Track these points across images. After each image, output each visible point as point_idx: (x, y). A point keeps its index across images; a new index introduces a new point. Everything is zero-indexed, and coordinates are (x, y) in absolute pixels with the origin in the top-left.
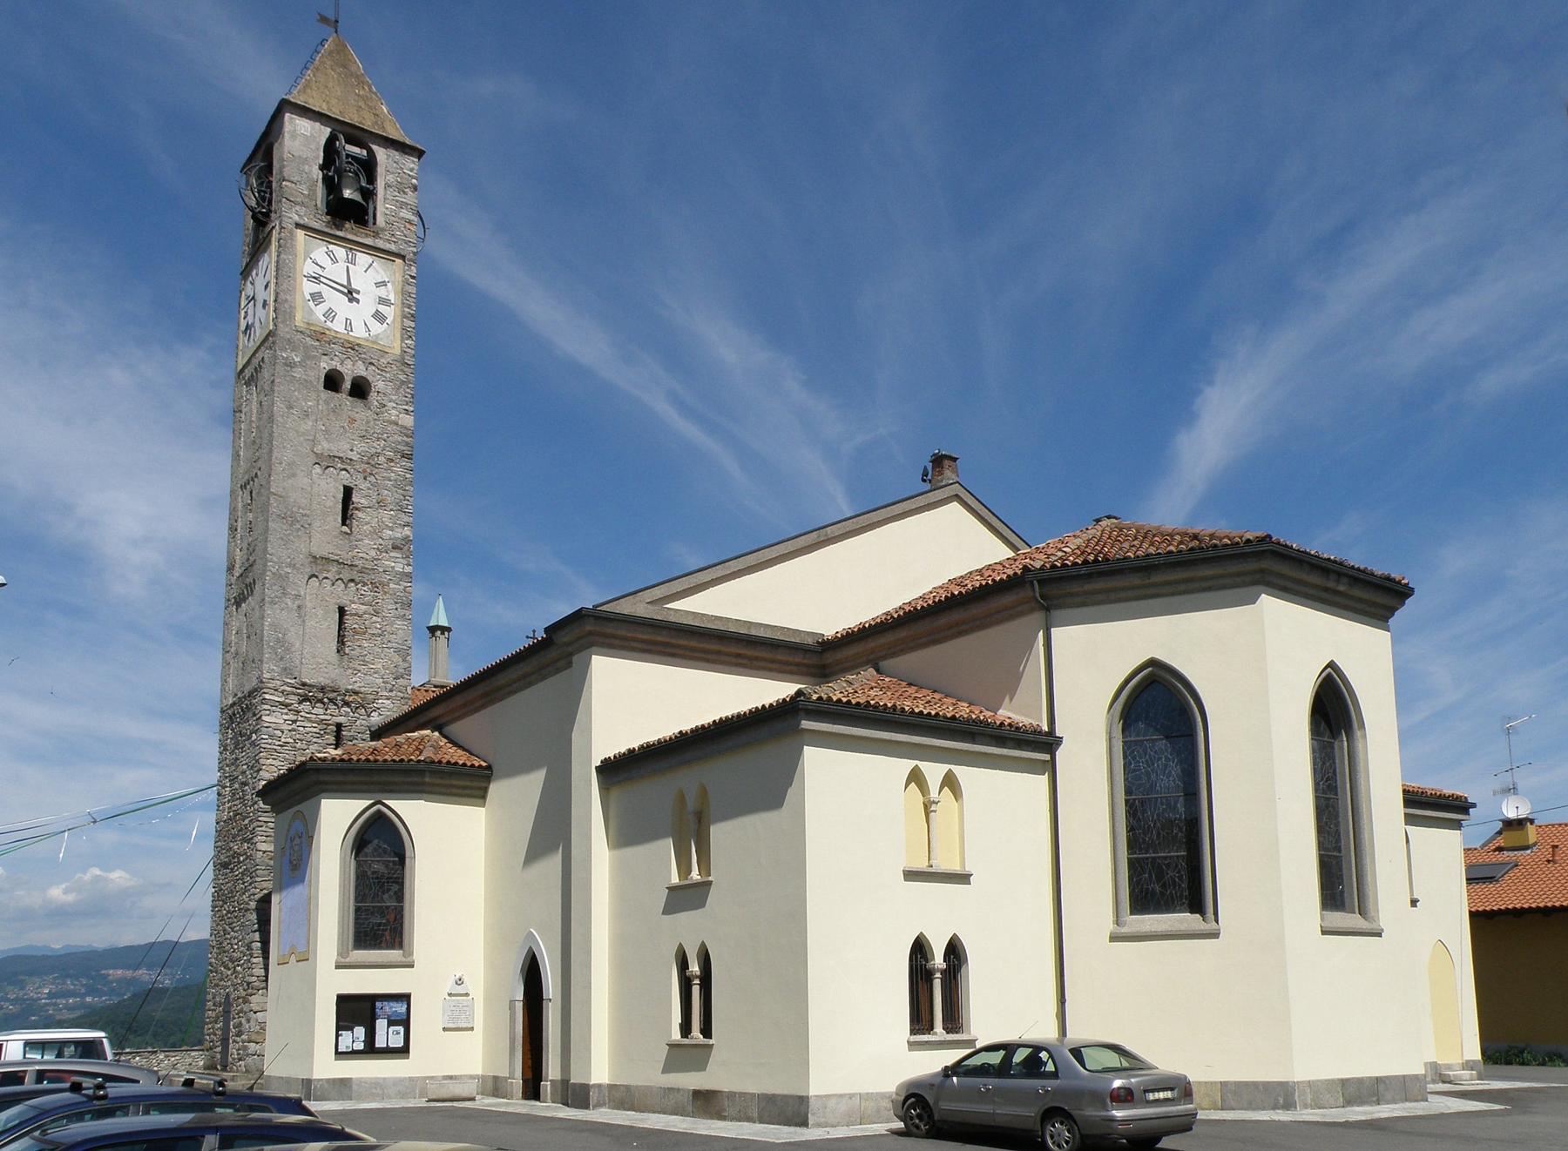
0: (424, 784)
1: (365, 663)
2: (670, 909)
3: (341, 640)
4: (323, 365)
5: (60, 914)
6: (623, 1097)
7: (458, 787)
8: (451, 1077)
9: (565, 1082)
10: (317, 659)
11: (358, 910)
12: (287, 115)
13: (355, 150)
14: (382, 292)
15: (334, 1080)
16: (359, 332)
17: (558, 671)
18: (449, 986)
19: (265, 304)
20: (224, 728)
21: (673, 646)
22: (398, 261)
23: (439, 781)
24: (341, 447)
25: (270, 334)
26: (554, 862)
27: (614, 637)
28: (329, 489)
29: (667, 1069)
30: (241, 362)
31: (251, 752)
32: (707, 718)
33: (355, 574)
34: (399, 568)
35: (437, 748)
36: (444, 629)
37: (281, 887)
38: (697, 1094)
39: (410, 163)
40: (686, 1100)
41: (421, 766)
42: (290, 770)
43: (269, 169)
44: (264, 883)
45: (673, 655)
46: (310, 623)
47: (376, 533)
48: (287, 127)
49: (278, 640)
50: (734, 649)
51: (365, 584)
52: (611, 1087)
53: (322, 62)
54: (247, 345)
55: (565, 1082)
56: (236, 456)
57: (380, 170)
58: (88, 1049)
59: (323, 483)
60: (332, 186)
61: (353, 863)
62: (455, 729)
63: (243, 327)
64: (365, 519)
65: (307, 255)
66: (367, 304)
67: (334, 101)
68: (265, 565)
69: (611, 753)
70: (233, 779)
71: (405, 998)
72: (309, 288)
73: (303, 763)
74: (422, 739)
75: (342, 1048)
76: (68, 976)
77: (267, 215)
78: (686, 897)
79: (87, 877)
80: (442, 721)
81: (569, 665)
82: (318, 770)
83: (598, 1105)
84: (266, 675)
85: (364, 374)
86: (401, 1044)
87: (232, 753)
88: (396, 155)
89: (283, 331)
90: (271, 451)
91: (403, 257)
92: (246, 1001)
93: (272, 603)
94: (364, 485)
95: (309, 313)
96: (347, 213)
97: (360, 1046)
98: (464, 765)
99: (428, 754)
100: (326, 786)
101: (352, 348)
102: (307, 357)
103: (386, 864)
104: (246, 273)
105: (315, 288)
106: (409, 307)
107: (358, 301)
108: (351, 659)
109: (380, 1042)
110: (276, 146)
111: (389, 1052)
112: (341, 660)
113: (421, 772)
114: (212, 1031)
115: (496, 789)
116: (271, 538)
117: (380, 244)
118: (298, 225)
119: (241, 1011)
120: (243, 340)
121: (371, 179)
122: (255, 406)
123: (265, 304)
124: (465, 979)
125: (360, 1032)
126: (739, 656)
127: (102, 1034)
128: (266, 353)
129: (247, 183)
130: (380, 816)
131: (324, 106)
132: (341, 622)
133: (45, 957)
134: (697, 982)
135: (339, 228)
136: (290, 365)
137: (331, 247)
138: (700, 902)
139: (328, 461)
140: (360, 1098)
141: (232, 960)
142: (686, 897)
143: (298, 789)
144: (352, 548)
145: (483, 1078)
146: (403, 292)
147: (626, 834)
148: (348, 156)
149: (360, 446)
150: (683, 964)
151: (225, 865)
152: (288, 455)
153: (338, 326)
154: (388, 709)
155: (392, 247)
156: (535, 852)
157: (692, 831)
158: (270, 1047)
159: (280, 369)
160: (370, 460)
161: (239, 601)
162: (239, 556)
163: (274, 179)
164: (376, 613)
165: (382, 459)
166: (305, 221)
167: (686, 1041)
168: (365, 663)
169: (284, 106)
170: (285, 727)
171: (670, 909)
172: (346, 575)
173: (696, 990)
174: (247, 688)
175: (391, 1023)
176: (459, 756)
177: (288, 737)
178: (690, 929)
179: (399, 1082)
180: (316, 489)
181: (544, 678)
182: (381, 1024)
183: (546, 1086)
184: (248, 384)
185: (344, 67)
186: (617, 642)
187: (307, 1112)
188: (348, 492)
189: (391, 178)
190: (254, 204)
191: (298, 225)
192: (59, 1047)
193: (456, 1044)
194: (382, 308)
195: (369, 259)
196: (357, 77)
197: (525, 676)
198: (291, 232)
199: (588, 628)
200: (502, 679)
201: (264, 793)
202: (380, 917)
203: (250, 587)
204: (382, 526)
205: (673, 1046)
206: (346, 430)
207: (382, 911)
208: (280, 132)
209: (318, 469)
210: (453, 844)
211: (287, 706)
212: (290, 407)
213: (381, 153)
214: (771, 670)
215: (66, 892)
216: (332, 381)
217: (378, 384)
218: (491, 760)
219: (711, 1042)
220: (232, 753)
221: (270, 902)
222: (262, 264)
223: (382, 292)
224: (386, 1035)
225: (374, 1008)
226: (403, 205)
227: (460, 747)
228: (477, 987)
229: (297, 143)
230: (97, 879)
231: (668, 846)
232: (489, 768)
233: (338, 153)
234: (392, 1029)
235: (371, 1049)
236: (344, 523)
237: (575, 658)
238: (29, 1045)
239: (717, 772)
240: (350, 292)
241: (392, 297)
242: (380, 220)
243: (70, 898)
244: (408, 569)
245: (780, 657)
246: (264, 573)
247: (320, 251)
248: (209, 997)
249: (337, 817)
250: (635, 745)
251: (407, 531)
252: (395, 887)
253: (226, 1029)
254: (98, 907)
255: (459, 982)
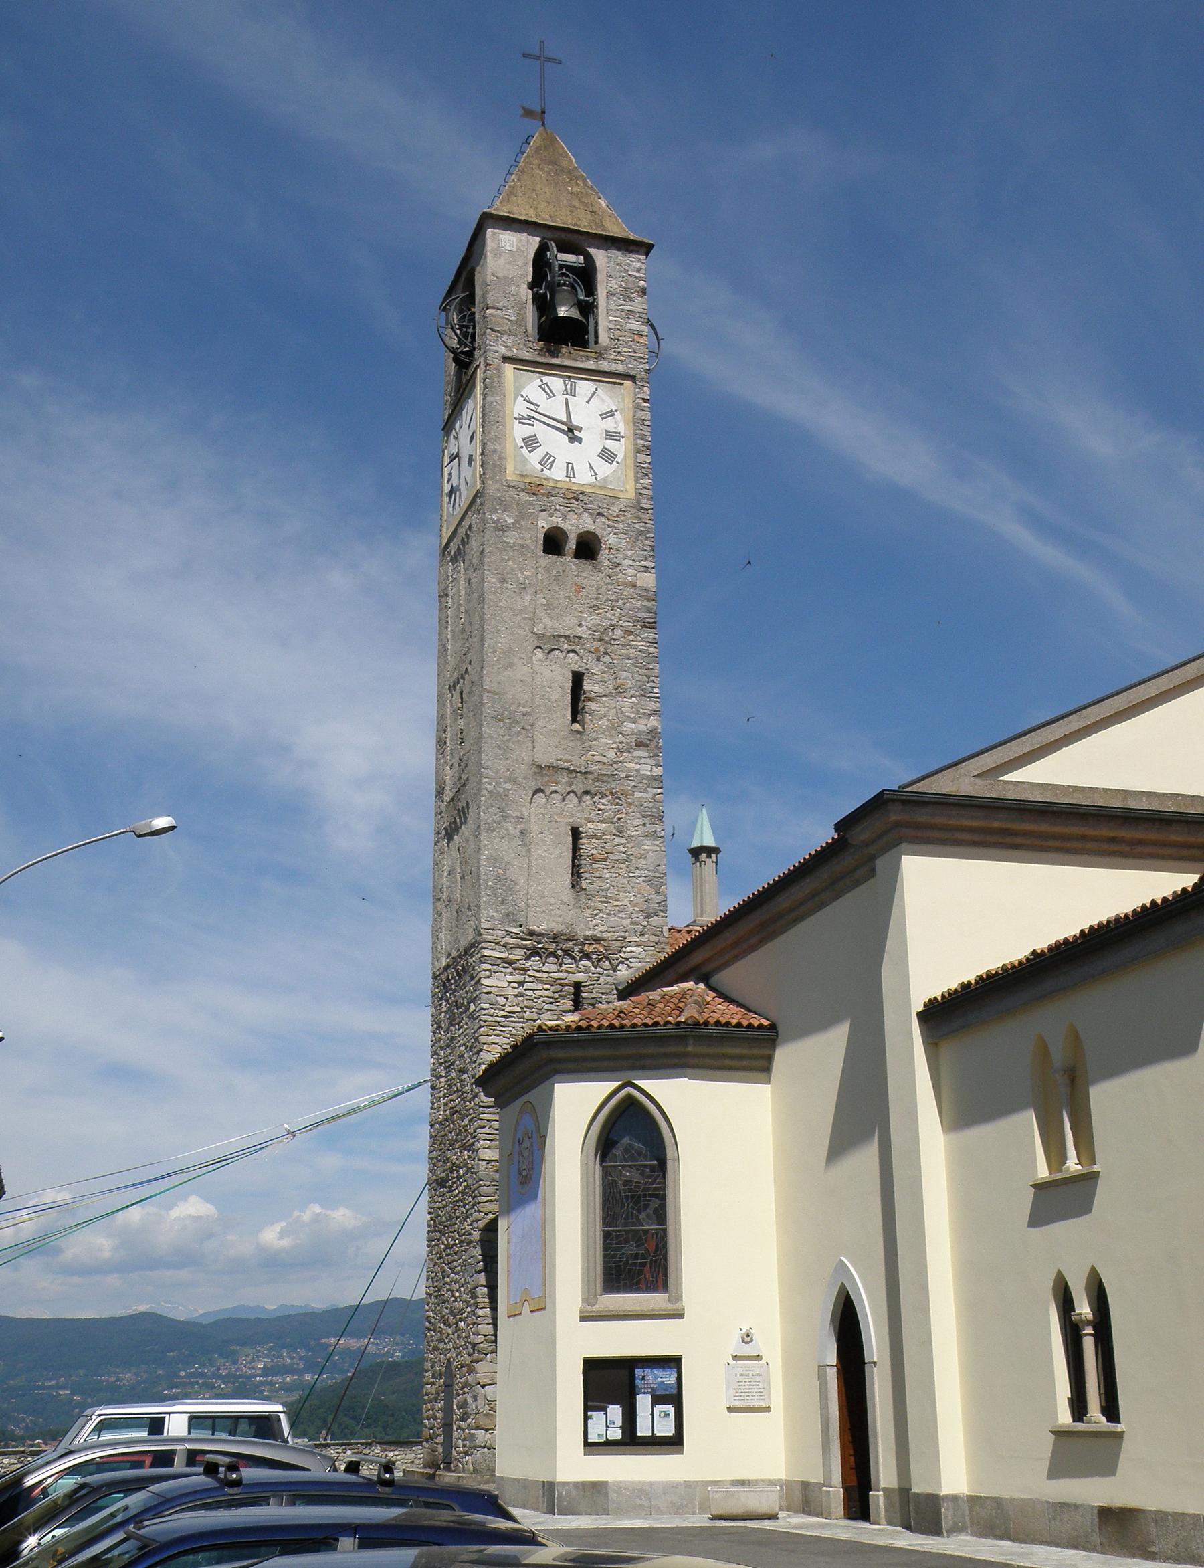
0: (686, 1055)
1: (608, 899)
2: (1039, 1217)
3: (576, 872)
4: (541, 523)
5: (273, 1264)
6: (993, 1517)
7: (732, 1057)
8: (742, 1483)
9: (904, 1492)
10: (548, 903)
11: (607, 1236)
12: (489, 231)
13: (570, 258)
14: (609, 424)
15: (584, 1484)
16: (583, 478)
17: (858, 883)
18: (734, 1345)
19: (471, 459)
20: (437, 999)
21: (1016, 833)
22: (628, 383)
23: (705, 1050)
24: (567, 623)
25: (478, 494)
26: (866, 1157)
27: (932, 827)
29: (1055, 1472)
30: (446, 534)
31: (468, 1027)
32: (1070, 928)
33: (590, 783)
34: (645, 770)
35: (702, 1005)
36: (710, 851)
37: (509, 1207)
38: (1107, 1515)
39: (636, 263)
40: (1089, 1523)
41: (682, 1030)
42: (514, 1047)
43: (471, 299)
44: (489, 1205)
45: (1016, 847)
46: (538, 852)
47: (615, 728)
48: (490, 245)
49: (498, 878)
50: (1105, 832)
51: (603, 796)
52: (973, 1500)
53: (527, 163)
54: (451, 512)
55: (904, 1492)
56: (443, 650)
57: (601, 277)
58: (263, 1426)
59: (546, 671)
60: (544, 305)
61: (598, 1168)
62: (728, 977)
63: (447, 489)
65: (518, 393)
66: (592, 441)
67: (543, 205)
68: (479, 783)
69: (937, 990)
70: (449, 1066)
71: (673, 1363)
72: (520, 432)
73: (530, 1036)
74: (682, 995)
75: (592, 1438)
76: (283, 1346)
77: (470, 354)
78: (1063, 1198)
79: (306, 1217)
80: (706, 969)
81: (872, 873)
82: (548, 1044)
83: (956, 1529)
84: (485, 925)
85: (591, 528)
86: (670, 1431)
87: (447, 1031)
88: (618, 255)
89: (493, 488)
90: (482, 638)
91: (632, 378)
92: (471, 1371)
93: (490, 829)
94: (596, 668)
95: (521, 463)
96: (563, 334)
97: (616, 1434)
98: (739, 1025)
99: (690, 1012)
100: (565, 1067)
101: (576, 497)
102: (522, 516)
103: (641, 1169)
104: (448, 427)
105: (527, 431)
106: (643, 437)
107: (580, 440)
108: (589, 896)
109: (643, 1430)
110: (478, 269)
111: (656, 1443)
112: (577, 899)
113: (682, 1039)
114: (432, 1410)
115: (783, 1055)
116: (485, 747)
117: (604, 365)
118: (506, 359)
119: (466, 1385)
120: (447, 507)
121: (590, 289)
122: (463, 584)
123: (471, 459)
124: (755, 1334)
125: (615, 1412)
126: (1113, 840)
127: (279, 1408)
128: (473, 519)
129: (447, 322)
130: (630, 1102)
131: (532, 212)
132: (575, 848)
133: (258, 1321)
134: (1089, 1331)
135: (554, 354)
136: (502, 528)
137: (546, 379)
138: (1083, 1206)
139: (550, 643)
140: (621, 1512)
141: (453, 1313)
142: (1063, 1198)
143: (524, 1072)
144: (585, 751)
145: (787, 1485)
146: (636, 422)
147: (967, 1109)
148: (561, 267)
149: (590, 620)
150: (1066, 1304)
151: (441, 1183)
152: (503, 641)
153: (557, 474)
154: (639, 958)
155: (619, 368)
156: (841, 1143)
157: (1062, 1097)
158: (501, 1437)
159: (490, 535)
160: (604, 636)
161: (450, 833)
162: (449, 775)
163: (476, 310)
164: (619, 832)
165: (618, 633)
166: (515, 352)
167: (1080, 1426)
168: (608, 899)
170: (510, 992)
171: (1039, 1217)
172: (579, 787)
173: (1089, 1344)
174: (463, 944)
175: (657, 1400)
176: (731, 1014)
177: (517, 1000)
178: (1072, 1247)
179: (670, 1488)
180: (538, 681)
182: (643, 1402)
183: (877, 1497)
184: (454, 560)
185: (554, 163)
186: (937, 834)
187: (510, 1517)
189: (614, 284)
190: (454, 342)
191: (506, 359)
192: (233, 1423)
193: (749, 1436)
194: (610, 444)
195: (591, 386)
196: (569, 172)
197: (813, 895)
198: (498, 369)
199: (894, 817)
200: (783, 902)
201: (484, 1081)
202: (636, 1251)
203: (463, 813)
204: (622, 718)
205: (1061, 1434)
206: (576, 602)
207: (639, 1238)
208: (482, 253)
209: (539, 654)
210: (731, 1140)
211: (511, 963)
212: (505, 581)
213: (600, 257)
214: (1163, 857)
215: (282, 1235)
216: (553, 543)
217: (609, 539)
218: (774, 1019)
219: (1120, 1427)
220: (447, 1031)
222: (466, 413)
223: (609, 424)
224: (653, 1419)
225: (632, 1377)
226: (630, 314)
227: (732, 1001)
228: (771, 1345)
229: (501, 262)
230: (317, 1219)
231: (1028, 1122)
232: (773, 1027)
233: (549, 265)
234: (658, 1408)
235: (631, 1440)
236: (574, 720)
237: (880, 863)
238: (196, 1420)
239: (1089, 1008)
240: (570, 430)
241: (621, 429)
242: (603, 338)
243: (285, 1243)
244: (658, 771)
245: (1174, 837)
246: (478, 793)
247: (533, 387)
248: (428, 1365)
249: (576, 1105)
250: (971, 977)
251: (654, 722)
252: (655, 1203)
253: (448, 1410)
254: (318, 1256)
255: (747, 1338)
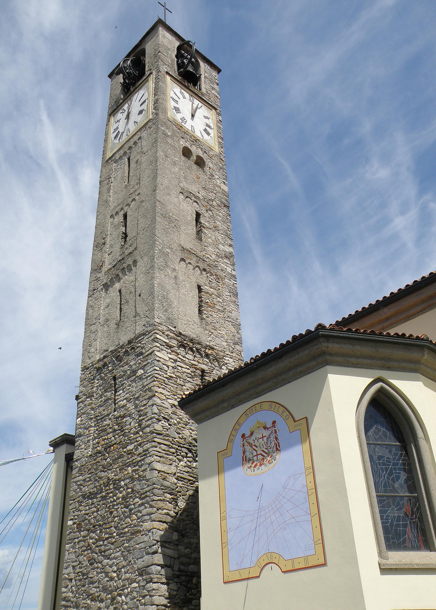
3: (200, 312)
24: (194, 189)
28: (188, 209)
64: (209, 235)
169: (160, 23)
181: (431, 309)
188: (198, 215)
209: (181, 196)
211: (170, 347)
217: (209, 163)
221: (143, 53)
241: (212, 125)
